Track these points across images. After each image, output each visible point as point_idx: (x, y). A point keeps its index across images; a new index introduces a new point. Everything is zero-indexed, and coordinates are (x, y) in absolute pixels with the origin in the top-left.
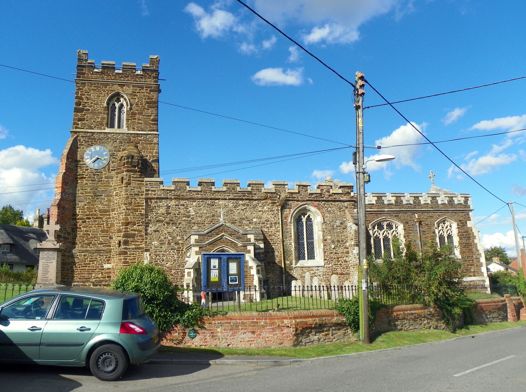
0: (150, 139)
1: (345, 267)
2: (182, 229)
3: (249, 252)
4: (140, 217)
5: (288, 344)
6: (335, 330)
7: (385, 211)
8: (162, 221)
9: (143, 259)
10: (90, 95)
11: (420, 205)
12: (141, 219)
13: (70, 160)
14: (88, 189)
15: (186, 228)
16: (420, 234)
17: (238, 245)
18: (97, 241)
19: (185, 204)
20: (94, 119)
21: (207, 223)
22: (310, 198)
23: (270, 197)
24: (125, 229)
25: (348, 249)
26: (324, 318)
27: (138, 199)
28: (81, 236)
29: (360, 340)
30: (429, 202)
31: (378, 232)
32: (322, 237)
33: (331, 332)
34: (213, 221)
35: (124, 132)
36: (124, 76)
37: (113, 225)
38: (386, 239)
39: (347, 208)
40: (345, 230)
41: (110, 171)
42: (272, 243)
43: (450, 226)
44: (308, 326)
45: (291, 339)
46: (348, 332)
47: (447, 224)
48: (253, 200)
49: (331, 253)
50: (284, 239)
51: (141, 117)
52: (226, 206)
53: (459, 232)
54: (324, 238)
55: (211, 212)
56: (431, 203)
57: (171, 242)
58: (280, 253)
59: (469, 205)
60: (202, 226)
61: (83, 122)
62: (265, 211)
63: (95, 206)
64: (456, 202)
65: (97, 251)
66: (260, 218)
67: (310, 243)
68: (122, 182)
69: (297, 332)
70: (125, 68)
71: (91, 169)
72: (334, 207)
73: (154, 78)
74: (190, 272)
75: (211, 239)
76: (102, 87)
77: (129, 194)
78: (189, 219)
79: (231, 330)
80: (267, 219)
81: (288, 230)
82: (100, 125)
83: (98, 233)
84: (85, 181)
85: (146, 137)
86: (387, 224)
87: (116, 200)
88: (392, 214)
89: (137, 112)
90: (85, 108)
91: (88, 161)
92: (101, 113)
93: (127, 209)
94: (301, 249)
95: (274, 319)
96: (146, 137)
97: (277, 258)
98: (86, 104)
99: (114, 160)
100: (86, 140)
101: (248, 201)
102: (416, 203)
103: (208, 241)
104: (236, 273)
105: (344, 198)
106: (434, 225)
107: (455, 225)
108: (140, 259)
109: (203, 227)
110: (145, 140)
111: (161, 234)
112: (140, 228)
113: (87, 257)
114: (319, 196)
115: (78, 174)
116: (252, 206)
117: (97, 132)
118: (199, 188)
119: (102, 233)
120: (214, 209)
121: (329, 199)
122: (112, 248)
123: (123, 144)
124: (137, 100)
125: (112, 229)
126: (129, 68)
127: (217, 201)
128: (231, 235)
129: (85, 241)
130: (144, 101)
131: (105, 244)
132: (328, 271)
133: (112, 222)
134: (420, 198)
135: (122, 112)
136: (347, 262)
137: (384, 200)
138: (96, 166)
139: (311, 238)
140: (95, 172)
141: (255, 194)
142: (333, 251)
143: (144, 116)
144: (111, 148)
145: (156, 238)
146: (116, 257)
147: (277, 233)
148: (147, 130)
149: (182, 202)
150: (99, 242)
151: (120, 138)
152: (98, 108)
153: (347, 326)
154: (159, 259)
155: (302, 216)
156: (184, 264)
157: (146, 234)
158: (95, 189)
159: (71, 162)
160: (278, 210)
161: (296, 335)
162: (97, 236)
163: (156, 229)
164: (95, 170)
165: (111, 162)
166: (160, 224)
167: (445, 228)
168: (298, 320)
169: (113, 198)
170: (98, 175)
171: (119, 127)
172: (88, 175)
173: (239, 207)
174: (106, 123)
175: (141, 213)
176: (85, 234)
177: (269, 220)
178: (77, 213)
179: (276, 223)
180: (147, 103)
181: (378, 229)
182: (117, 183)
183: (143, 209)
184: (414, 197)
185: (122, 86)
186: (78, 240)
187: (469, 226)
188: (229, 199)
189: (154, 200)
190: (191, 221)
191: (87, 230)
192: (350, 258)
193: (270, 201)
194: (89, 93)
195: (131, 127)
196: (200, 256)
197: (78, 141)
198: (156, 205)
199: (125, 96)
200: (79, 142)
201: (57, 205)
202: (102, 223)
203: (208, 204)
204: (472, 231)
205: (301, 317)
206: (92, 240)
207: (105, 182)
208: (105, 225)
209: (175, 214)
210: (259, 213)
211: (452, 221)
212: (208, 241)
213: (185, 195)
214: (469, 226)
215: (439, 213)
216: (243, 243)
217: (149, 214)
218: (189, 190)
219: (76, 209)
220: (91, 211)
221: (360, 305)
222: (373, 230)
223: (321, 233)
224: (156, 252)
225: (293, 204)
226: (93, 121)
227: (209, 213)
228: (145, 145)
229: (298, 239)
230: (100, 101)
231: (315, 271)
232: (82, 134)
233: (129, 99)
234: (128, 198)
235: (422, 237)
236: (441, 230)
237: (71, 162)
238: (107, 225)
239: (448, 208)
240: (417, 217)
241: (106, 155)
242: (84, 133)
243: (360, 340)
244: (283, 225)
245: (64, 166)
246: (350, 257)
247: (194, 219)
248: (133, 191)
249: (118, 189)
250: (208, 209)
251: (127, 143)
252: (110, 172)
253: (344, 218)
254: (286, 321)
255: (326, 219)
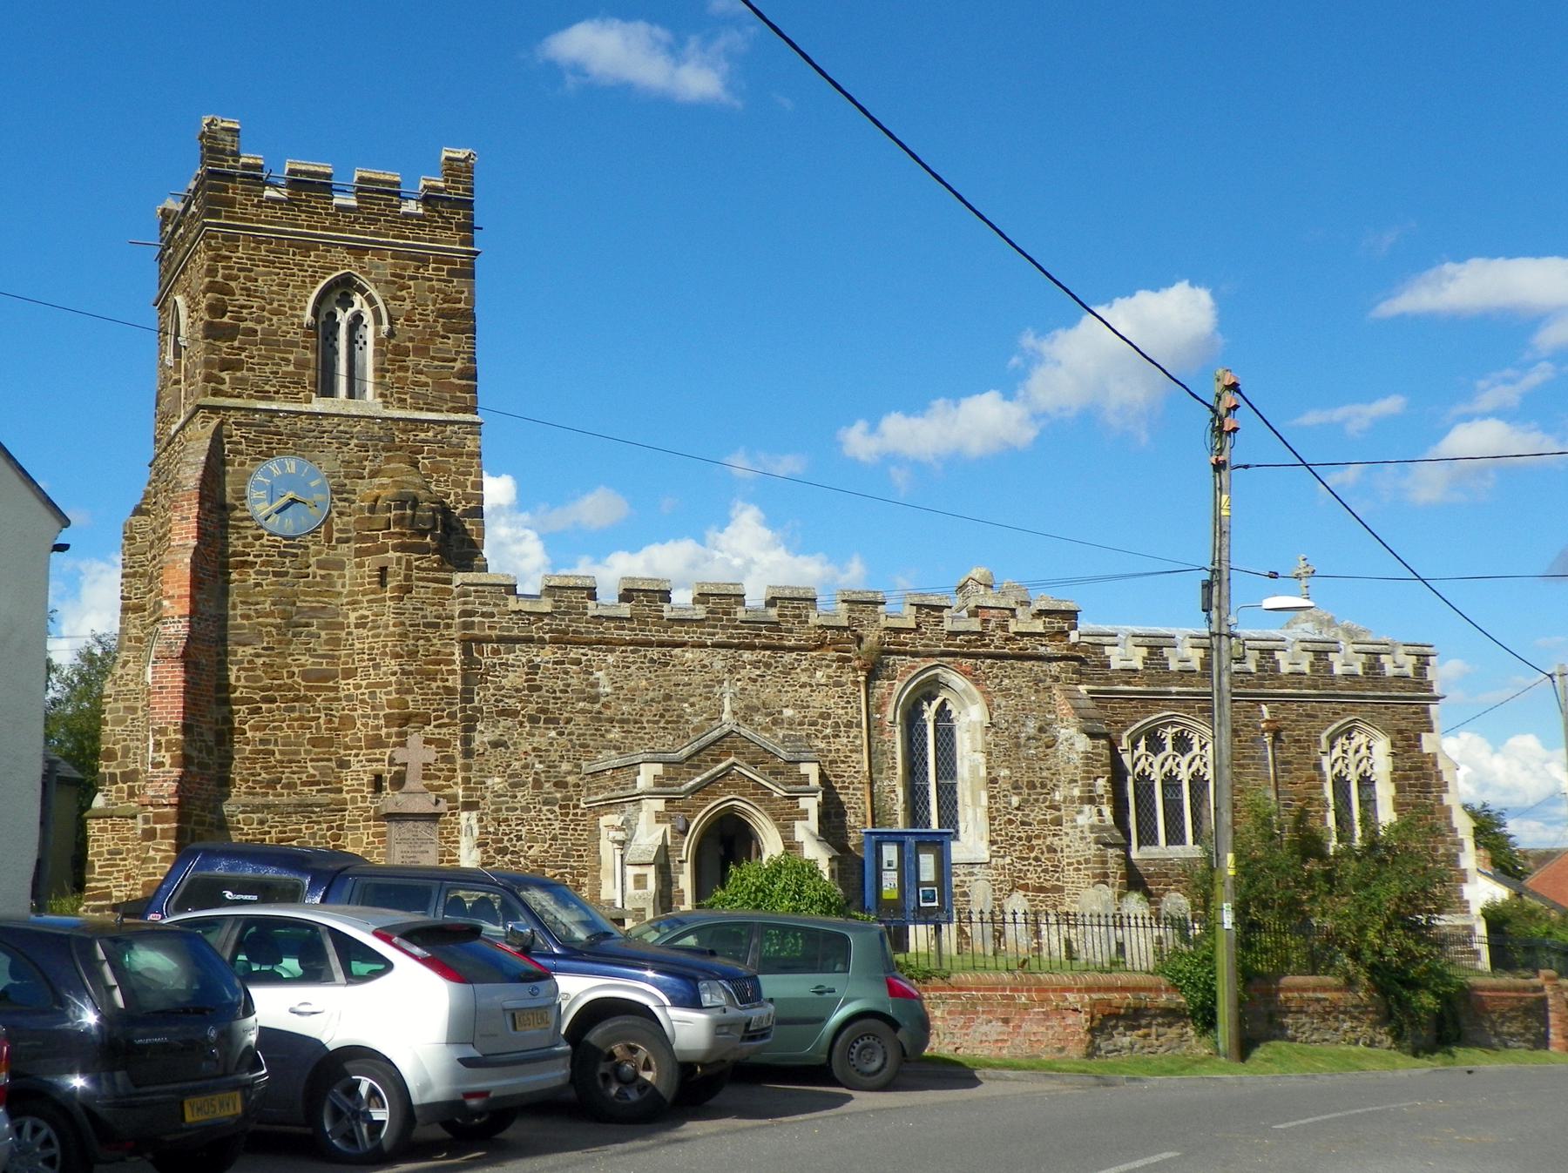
0: (454, 440)
1: (1051, 869)
2: (574, 737)
3: (804, 815)
4: (442, 699)
5: (1075, 1051)
6: (1162, 1025)
7: (1170, 693)
8: (515, 713)
9: (456, 834)
10: (256, 280)
11: (1279, 678)
12: (447, 703)
13: (208, 505)
14: (264, 602)
15: (587, 737)
16: (1275, 771)
17: (775, 795)
18: (300, 776)
19: (584, 658)
20: (273, 364)
21: (648, 722)
22: (949, 645)
23: (834, 642)
24: (396, 737)
25: (1059, 810)
26: (1142, 995)
27: (435, 641)
28: (248, 758)
29: (1218, 1053)
30: (1306, 668)
31: (1147, 759)
32: (983, 772)
33: (1154, 1030)
34: (667, 715)
35: (372, 414)
36: (365, 219)
37: (347, 722)
38: (1171, 782)
39: (1057, 679)
40: (1052, 750)
41: (334, 543)
42: (838, 785)
43: (1369, 748)
44: (1114, 1010)
45: (1081, 1040)
46: (1187, 1033)
47: (1359, 739)
48: (783, 648)
49: (1011, 822)
50: (874, 776)
51: (423, 363)
52: (705, 666)
53: (1396, 769)
54: (989, 773)
55: (660, 687)
56: (1312, 671)
57: (543, 779)
58: (862, 818)
59: (1431, 682)
60: (636, 730)
61: (239, 374)
62: (818, 685)
63: (289, 660)
64: (1390, 670)
65: (299, 805)
66: (804, 707)
67: (946, 788)
68: (383, 583)
69: (1094, 1024)
70: (366, 189)
71: (269, 535)
72: (1018, 677)
73: (460, 227)
74: (646, 875)
75: (698, 775)
76: (294, 254)
77: (408, 623)
78: (597, 706)
79: (961, 1013)
80: (824, 710)
81: (885, 748)
82: (291, 386)
83: (302, 749)
84: (253, 576)
85: (442, 432)
86: (1176, 733)
87: (362, 641)
88: (1191, 703)
89: (410, 345)
90: (243, 325)
91: (259, 505)
92: (295, 344)
93: (404, 672)
94: (920, 808)
95: (1046, 991)
96: (442, 432)
97: (851, 835)
98: (245, 311)
99: (345, 507)
100: (251, 436)
101: (768, 652)
102: (1266, 671)
103: (690, 780)
104: (933, 879)
105: (1050, 650)
106: (1318, 742)
107: (1382, 746)
108: (448, 833)
109: (637, 733)
110: (439, 442)
111: (512, 753)
112: (444, 735)
113: (271, 827)
114: (976, 640)
115: (231, 550)
116: (780, 669)
117: (286, 411)
118: (625, 610)
119: (314, 746)
120: (668, 675)
121: (1006, 650)
122: (348, 797)
123: (371, 453)
124: (408, 305)
125: (346, 736)
126: (378, 191)
127: (677, 651)
128: (754, 764)
129: (260, 775)
130: (431, 307)
131: (326, 783)
132: (1002, 878)
133: (346, 712)
134: (1278, 655)
135: (357, 342)
136: (1055, 851)
137: (1166, 659)
138: (287, 524)
139: (949, 773)
140: (285, 546)
141: (790, 631)
142: (1016, 815)
143: (433, 358)
144: (336, 466)
145: (497, 766)
146: (365, 828)
147: (854, 755)
148: (444, 409)
149: (574, 653)
150: (305, 779)
151: (360, 432)
152: (284, 328)
153: (1188, 1017)
154: (506, 834)
155: (925, 703)
156: (582, 848)
157: (468, 753)
158: (287, 604)
159: (209, 511)
160: (856, 683)
161: (1091, 1030)
162: (299, 758)
163: (497, 738)
164: (285, 539)
165: (334, 514)
166: (509, 722)
167: (1351, 753)
168: (1095, 996)
169: (349, 634)
170: (295, 555)
171: (351, 394)
172: (261, 556)
173: (743, 672)
174: (314, 380)
175: (447, 684)
176: (260, 751)
177: (829, 715)
178: (232, 680)
179: (849, 725)
180: (442, 314)
181: (1147, 750)
182: (362, 585)
183: (453, 672)
184: (1261, 651)
185: (358, 251)
186: (238, 770)
187: (1426, 750)
188: (715, 645)
189: (490, 645)
190: (600, 713)
191: (267, 737)
192: (1066, 840)
193: (834, 653)
194: (252, 274)
195: (392, 395)
196: (668, 826)
197: (225, 440)
198: (495, 661)
199: (372, 291)
200: (228, 443)
201: (182, 657)
202: (312, 715)
203: (652, 661)
204: (1435, 764)
205: (1099, 989)
206: (283, 773)
207: (318, 579)
208: (322, 721)
209: (555, 692)
210: (800, 690)
211: (1376, 732)
212: (692, 783)
213: (583, 630)
214: (1426, 750)
215: (1334, 705)
216: (790, 787)
217: (476, 690)
218: (596, 613)
219: (227, 669)
220: (275, 674)
221: (1219, 965)
222: (1133, 752)
223: (981, 758)
224: (498, 810)
225: (901, 664)
226: (271, 373)
227: (654, 690)
228: (439, 458)
229: (910, 773)
230: (289, 301)
231: (962, 878)
232: (239, 414)
233: (384, 300)
234: (404, 635)
235: (1280, 780)
236: (1340, 760)
237: (209, 511)
238: (330, 721)
239: (1363, 690)
240: (1267, 716)
241: (320, 488)
242: (243, 413)
243: (1218, 1053)
244: (872, 732)
245: (192, 525)
246: (1063, 837)
247: (609, 708)
248: (421, 613)
249: (365, 605)
250: (652, 676)
251: (384, 449)
252: (335, 548)
253: (1050, 712)
254: (1071, 997)
255: (995, 714)
